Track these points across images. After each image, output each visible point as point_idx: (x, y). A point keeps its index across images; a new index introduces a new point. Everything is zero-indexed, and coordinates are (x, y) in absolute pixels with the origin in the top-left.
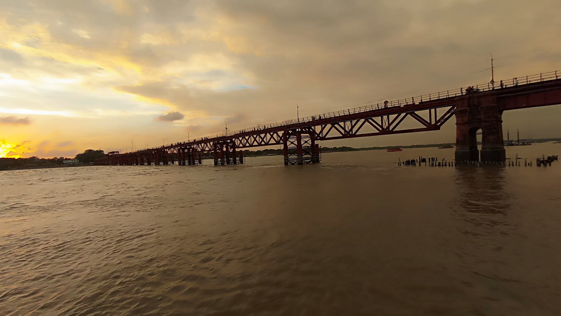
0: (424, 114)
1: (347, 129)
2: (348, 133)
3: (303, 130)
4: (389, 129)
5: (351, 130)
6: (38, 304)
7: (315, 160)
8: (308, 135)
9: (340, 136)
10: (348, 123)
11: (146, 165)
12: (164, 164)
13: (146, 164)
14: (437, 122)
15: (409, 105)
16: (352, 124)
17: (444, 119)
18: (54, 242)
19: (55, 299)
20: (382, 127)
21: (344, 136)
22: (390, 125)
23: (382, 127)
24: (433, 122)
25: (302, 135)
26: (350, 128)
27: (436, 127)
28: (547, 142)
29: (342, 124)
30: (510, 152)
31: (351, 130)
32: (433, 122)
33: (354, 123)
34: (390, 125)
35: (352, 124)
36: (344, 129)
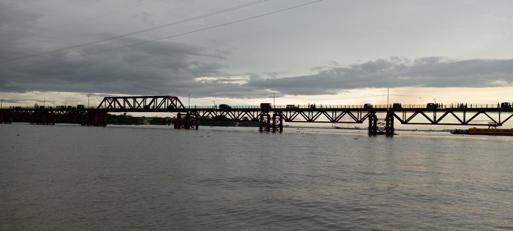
0: (355, 114)
1: (236, 116)
2: (236, 118)
3: (278, 114)
4: (290, 119)
5: (238, 117)
6: (285, 223)
7: (281, 131)
8: (267, 117)
9: (439, 122)
10: (256, 113)
11: (46, 125)
12: (31, 124)
13: (52, 124)
14: (361, 119)
15: (253, 109)
16: (239, 114)
17: (364, 119)
18: (323, 211)
19: (328, 216)
20: (308, 118)
21: (308, 121)
22: (313, 118)
23: (308, 118)
24: (359, 120)
25: (264, 117)
26: (237, 116)
27: (361, 122)
28: (438, 130)
29: (252, 113)
30: (395, 132)
31: (238, 117)
32: (359, 120)
33: (240, 113)
34: (313, 118)
35: (239, 114)
36: (253, 116)
